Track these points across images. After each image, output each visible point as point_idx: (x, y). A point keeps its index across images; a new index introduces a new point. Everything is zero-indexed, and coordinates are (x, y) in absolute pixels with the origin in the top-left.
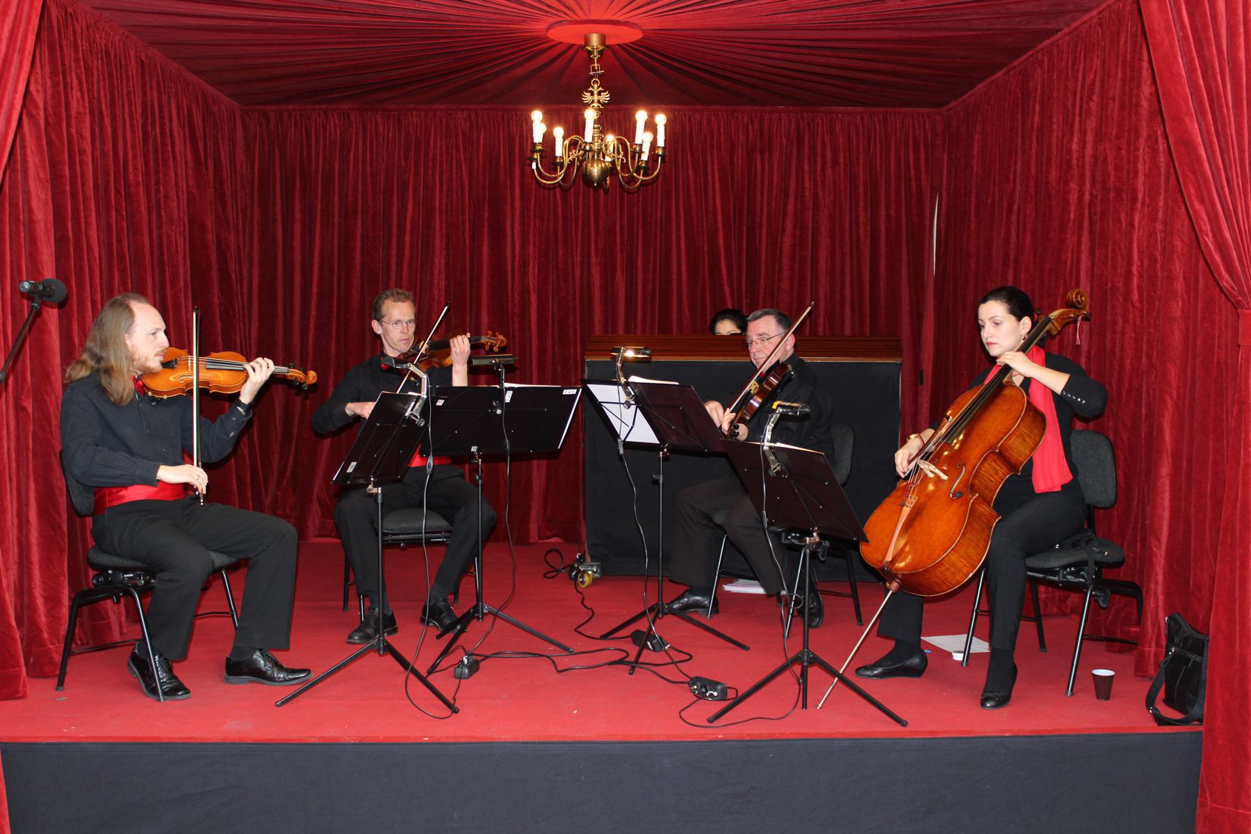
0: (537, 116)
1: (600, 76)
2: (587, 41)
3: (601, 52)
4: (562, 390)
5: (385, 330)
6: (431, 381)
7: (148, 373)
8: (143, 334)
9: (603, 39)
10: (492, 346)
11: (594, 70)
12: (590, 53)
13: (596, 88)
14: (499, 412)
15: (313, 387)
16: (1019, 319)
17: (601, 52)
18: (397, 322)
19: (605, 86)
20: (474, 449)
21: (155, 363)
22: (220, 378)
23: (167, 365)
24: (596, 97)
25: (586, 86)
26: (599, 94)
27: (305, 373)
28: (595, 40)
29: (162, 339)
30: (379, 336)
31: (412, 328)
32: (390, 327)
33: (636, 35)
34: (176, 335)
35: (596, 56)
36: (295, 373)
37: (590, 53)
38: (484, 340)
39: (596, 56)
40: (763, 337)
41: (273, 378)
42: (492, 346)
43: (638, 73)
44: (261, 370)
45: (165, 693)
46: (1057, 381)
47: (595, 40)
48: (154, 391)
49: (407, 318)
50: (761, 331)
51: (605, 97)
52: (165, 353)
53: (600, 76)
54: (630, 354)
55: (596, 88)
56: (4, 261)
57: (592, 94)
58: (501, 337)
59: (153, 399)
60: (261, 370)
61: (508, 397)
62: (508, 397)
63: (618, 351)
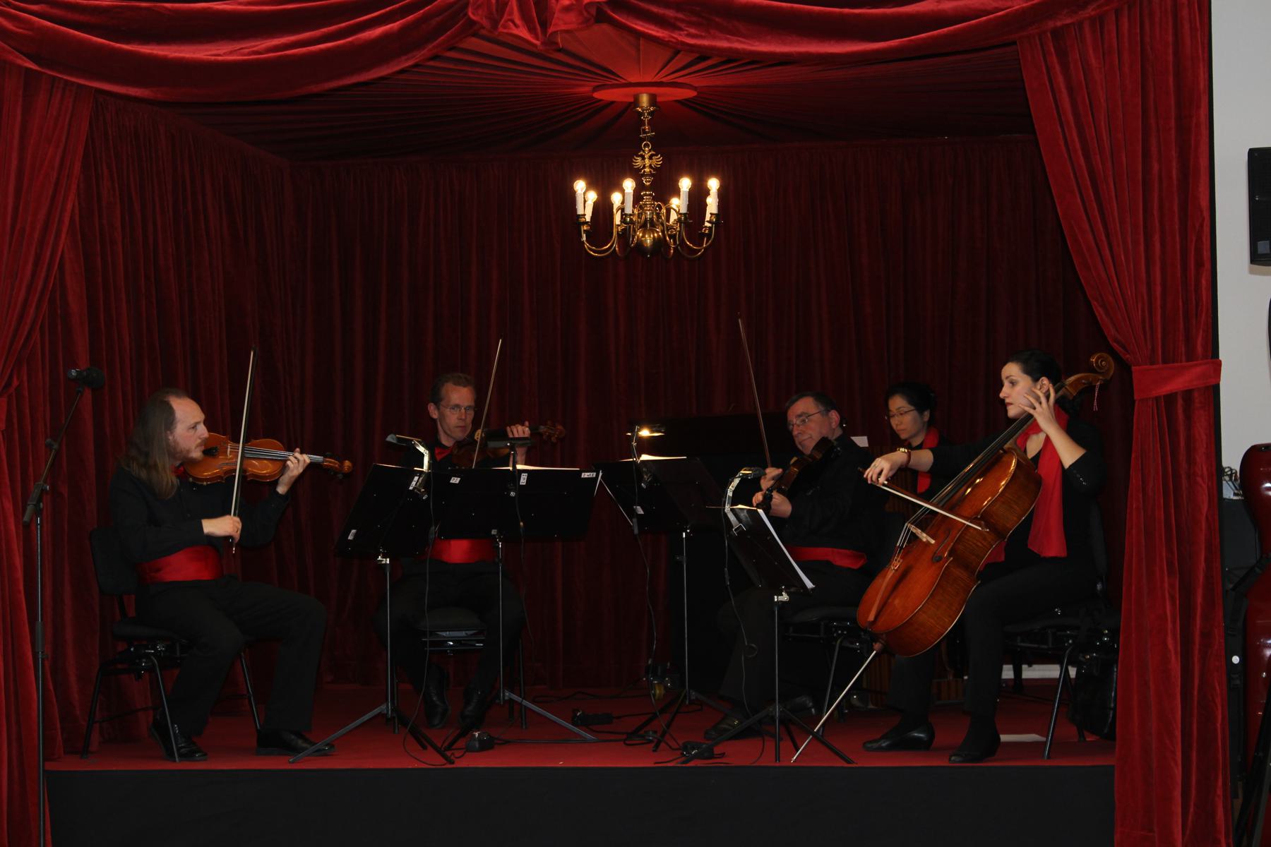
0: (580, 186)
1: (651, 139)
2: (636, 102)
3: (651, 114)
4: (579, 473)
5: (442, 415)
6: (432, 457)
7: (193, 462)
8: (187, 422)
9: (653, 101)
10: (550, 437)
11: (645, 132)
12: (641, 114)
13: (647, 152)
14: (512, 494)
15: (346, 475)
16: (1036, 380)
17: (651, 114)
18: (458, 406)
19: (657, 148)
20: (494, 532)
21: (197, 454)
22: (262, 468)
23: (210, 451)
24: (647, 162)
25: (637, 150)
26: (650, 158)
27: (342, 463)
28: (644, 100)
29: (202, 430)
30: (434, 421)
31: (471, 414)
32: (448, 412)
33: (691, 94)
34: (220, 421)
35: (646, 118)
36: (331, 462)
37: (641, 114)
38: (542, 429)
39: (646, 118)
40: (804, 416)
41: (311, 467)
42: (550, 437)
43: (686, 139)
44: (298, 462)
45: (181, 755)
46: (1069, 453)
47: (644, 100)
48: (194, 478)
49: (467, 403)
50: (799, 412)
51: (658, 161)
52: (205, 442)
53: (651, 139)
54: (645, 433)
55: (647, 152)
56: (328, 49)
57: (643, 158)
58: (560, 427)
59: (194, 484)
60: (298, 462)
61: (523, 480)
62: (523, 480)
63: (632, 431)
